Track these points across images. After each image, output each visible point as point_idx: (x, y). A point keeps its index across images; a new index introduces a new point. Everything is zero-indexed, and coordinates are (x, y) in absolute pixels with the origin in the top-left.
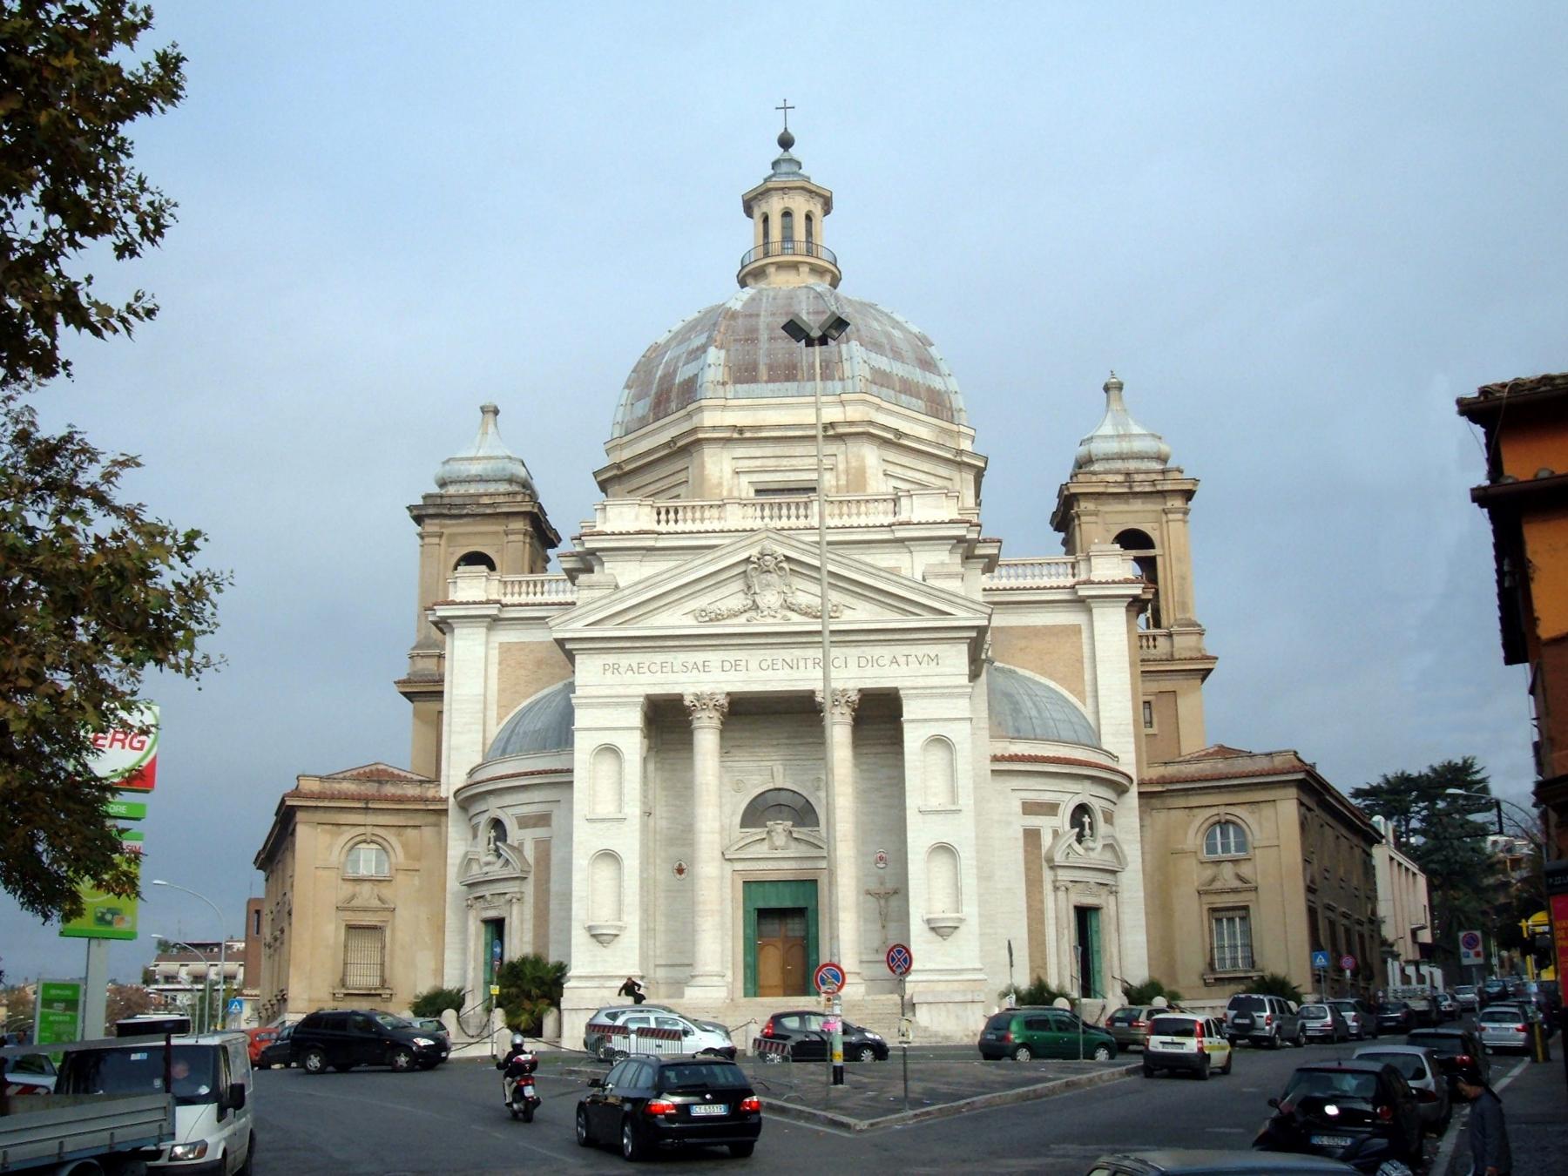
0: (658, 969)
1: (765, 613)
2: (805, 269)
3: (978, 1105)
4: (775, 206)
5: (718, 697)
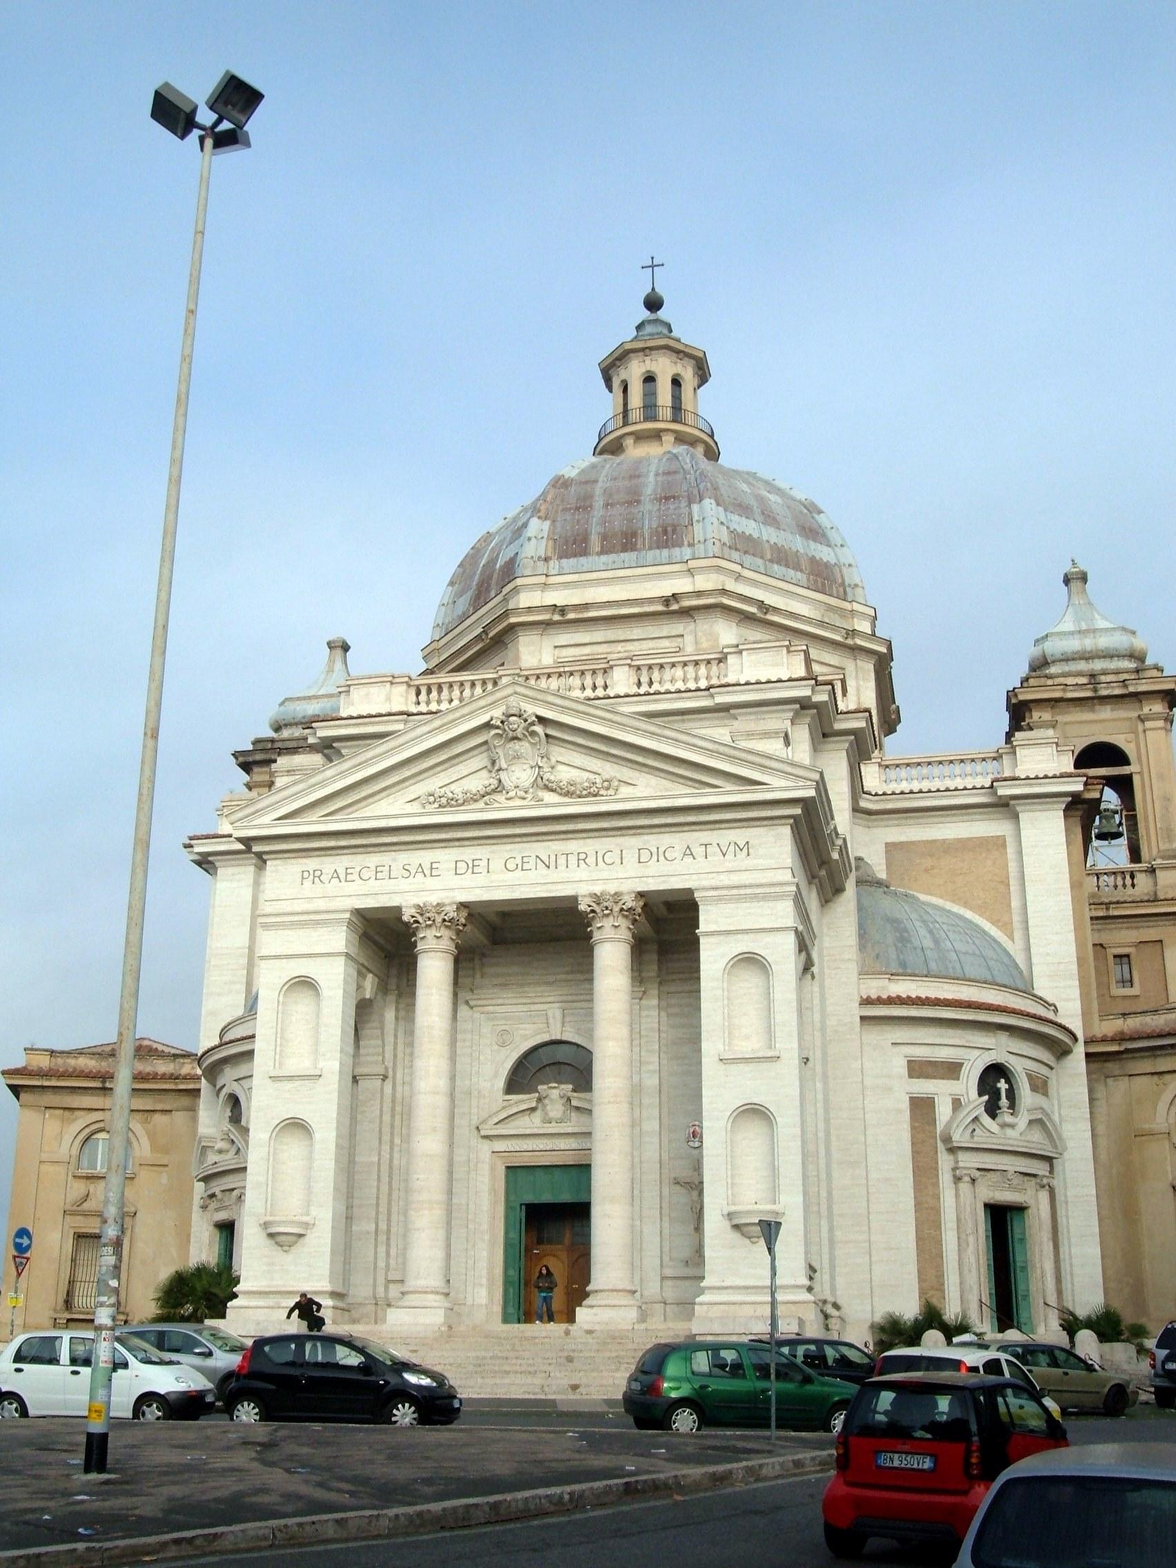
0: (391, 1286)
1: (512, 794)
2: (668, 439)
3: (226, 1544)
4: (635, 371)
5: (447, 908)
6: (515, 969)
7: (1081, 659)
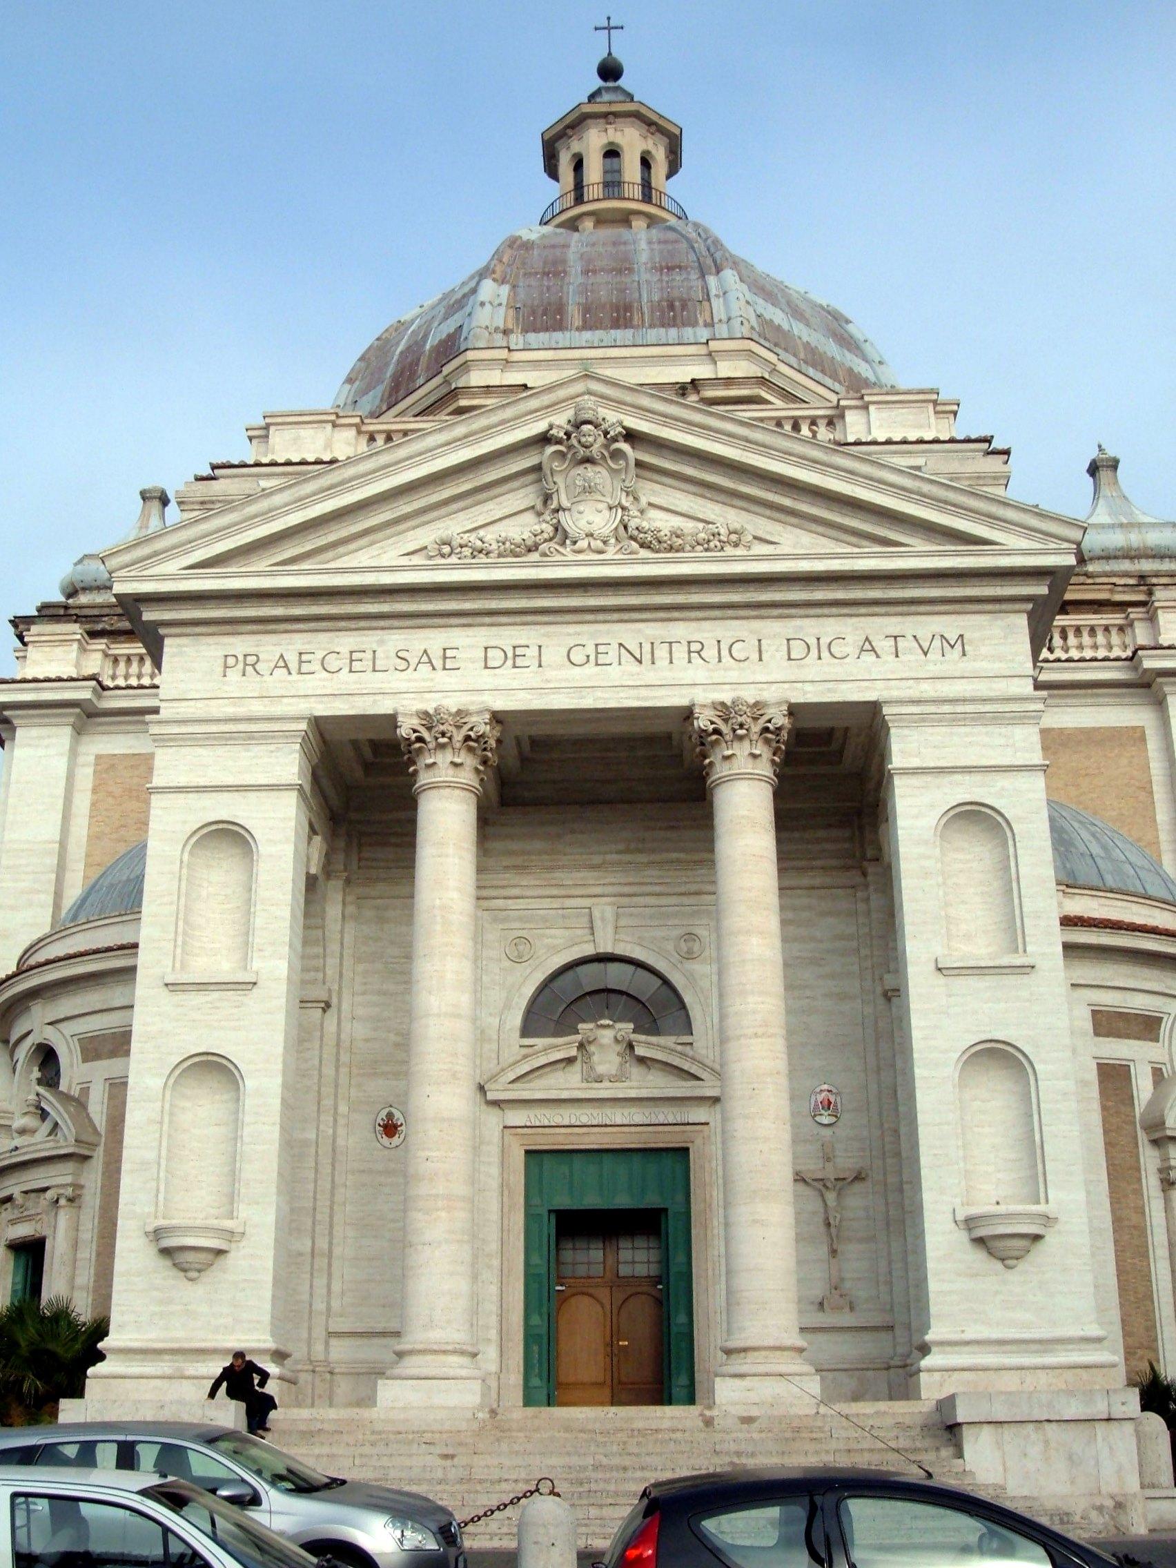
0: (334, 1342)
1: (582, 544)
4: (593, 141)
5: (474, 719)
6: (538, 845)
7: (1125, 557)
